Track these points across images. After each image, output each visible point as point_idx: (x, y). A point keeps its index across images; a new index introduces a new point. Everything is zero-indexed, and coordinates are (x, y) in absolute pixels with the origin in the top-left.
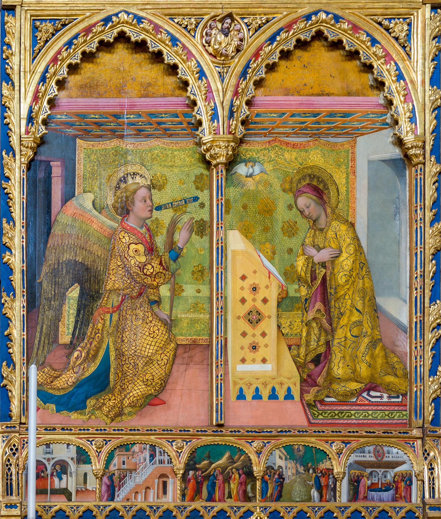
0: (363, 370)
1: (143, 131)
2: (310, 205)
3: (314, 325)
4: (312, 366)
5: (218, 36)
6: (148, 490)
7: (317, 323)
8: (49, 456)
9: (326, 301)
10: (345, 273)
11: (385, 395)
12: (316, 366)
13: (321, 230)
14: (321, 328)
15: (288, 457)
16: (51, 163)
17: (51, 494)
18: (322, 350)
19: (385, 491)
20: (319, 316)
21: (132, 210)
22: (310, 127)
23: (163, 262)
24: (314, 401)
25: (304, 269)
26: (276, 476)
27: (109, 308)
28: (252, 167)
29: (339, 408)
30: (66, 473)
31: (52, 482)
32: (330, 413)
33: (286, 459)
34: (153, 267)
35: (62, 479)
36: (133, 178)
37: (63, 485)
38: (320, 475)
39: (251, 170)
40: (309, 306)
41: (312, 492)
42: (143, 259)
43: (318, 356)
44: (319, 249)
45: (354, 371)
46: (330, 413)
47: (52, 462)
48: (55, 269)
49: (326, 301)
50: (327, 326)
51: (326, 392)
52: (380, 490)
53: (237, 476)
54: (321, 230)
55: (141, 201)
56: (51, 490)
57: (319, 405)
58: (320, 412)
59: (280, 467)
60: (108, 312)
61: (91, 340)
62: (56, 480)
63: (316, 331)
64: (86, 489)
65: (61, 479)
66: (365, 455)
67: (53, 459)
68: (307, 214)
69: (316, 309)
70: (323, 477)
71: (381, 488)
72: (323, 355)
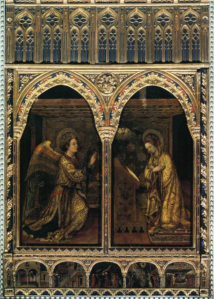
0: (175, 218)
1: (73, 113)
2: (151, 147)
3: (153, 199)
4: (152, 218)
5: (84, 182)
6: (74, 283)
7: (154, 199)
8: (27, 267)
9: (158, 189)
10: (167, 176)
11: (186, 230)
12: (154, 217)
13: (156, 158)
14: (156, 200)
15: (138, 267)
16: (31, 128)
17: (28, 284)
18: (156, 210)
19: (182, 282)
20: (155, 195)
21: (69, 149)
22: (151, 112)
23: (83, 171)
24: (154, 233)
25: (148, 175)
26: (133, 276)
27: (58, 192)
28: (124, 130)
29: (165, 236)
30: (35, 275)
31: (29, 279)
32: (161, 238)
33: (137, 268)
34: (78, 174)
35: (34, 277)
36: (69, 134)
37: (34, 280)
38: (152, 275)
39: (124, 131)
40: (150, 191)
41: (149, 283)
42: (73, 171)
43: (155, 213)
44: (155, 166)
45: (171, 218)
46: (161, 238)
47: (29, 270)
48: (33, 175)
49: (158, 189)
50: (159, 200)
51: (159, 229)
52: (180, 282)
53: (114, 276)
54: (156, 158)
55: (73, 145)
56: (29, 282)
57: (155, 235)
58: (156, 238)
59: (134, 272)
60: (58, 194)
61: (50, 206)
62: (31, 278)
63: (154, 202)
64: (45, 282)
65: (33, 277)
66: (174, 266)
67: (29, 268)
68: (150, 150)
69: (154, 192)
70: (154, 276)
71: (181, 281)
72: (157, 213)
